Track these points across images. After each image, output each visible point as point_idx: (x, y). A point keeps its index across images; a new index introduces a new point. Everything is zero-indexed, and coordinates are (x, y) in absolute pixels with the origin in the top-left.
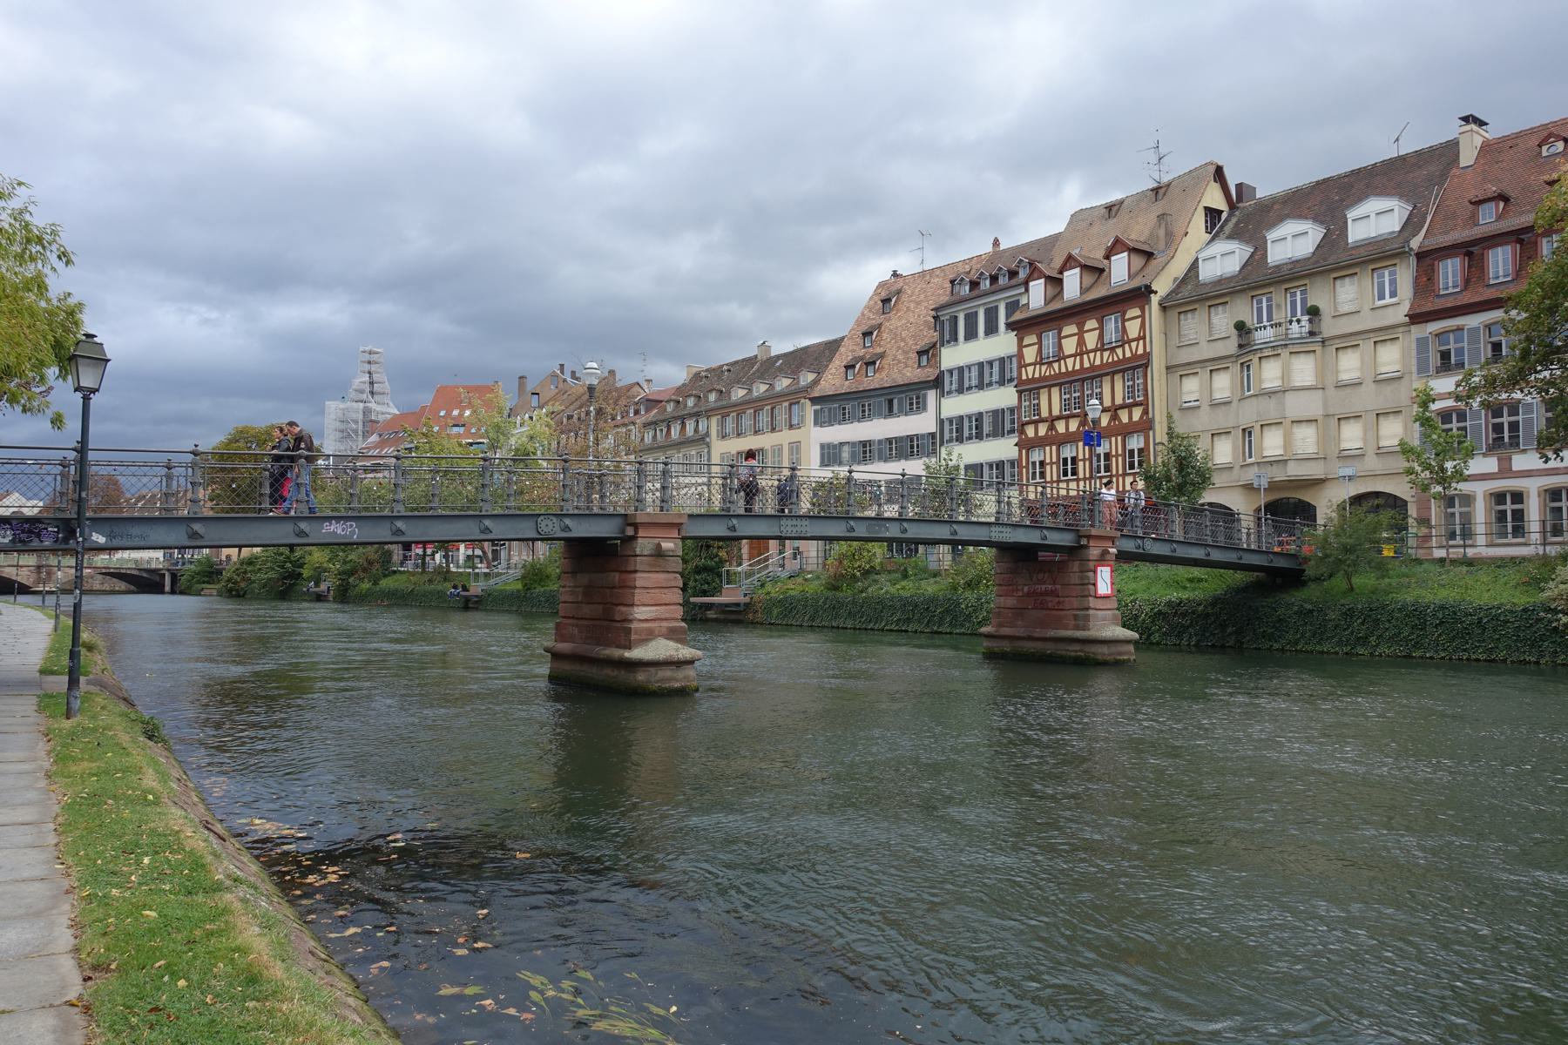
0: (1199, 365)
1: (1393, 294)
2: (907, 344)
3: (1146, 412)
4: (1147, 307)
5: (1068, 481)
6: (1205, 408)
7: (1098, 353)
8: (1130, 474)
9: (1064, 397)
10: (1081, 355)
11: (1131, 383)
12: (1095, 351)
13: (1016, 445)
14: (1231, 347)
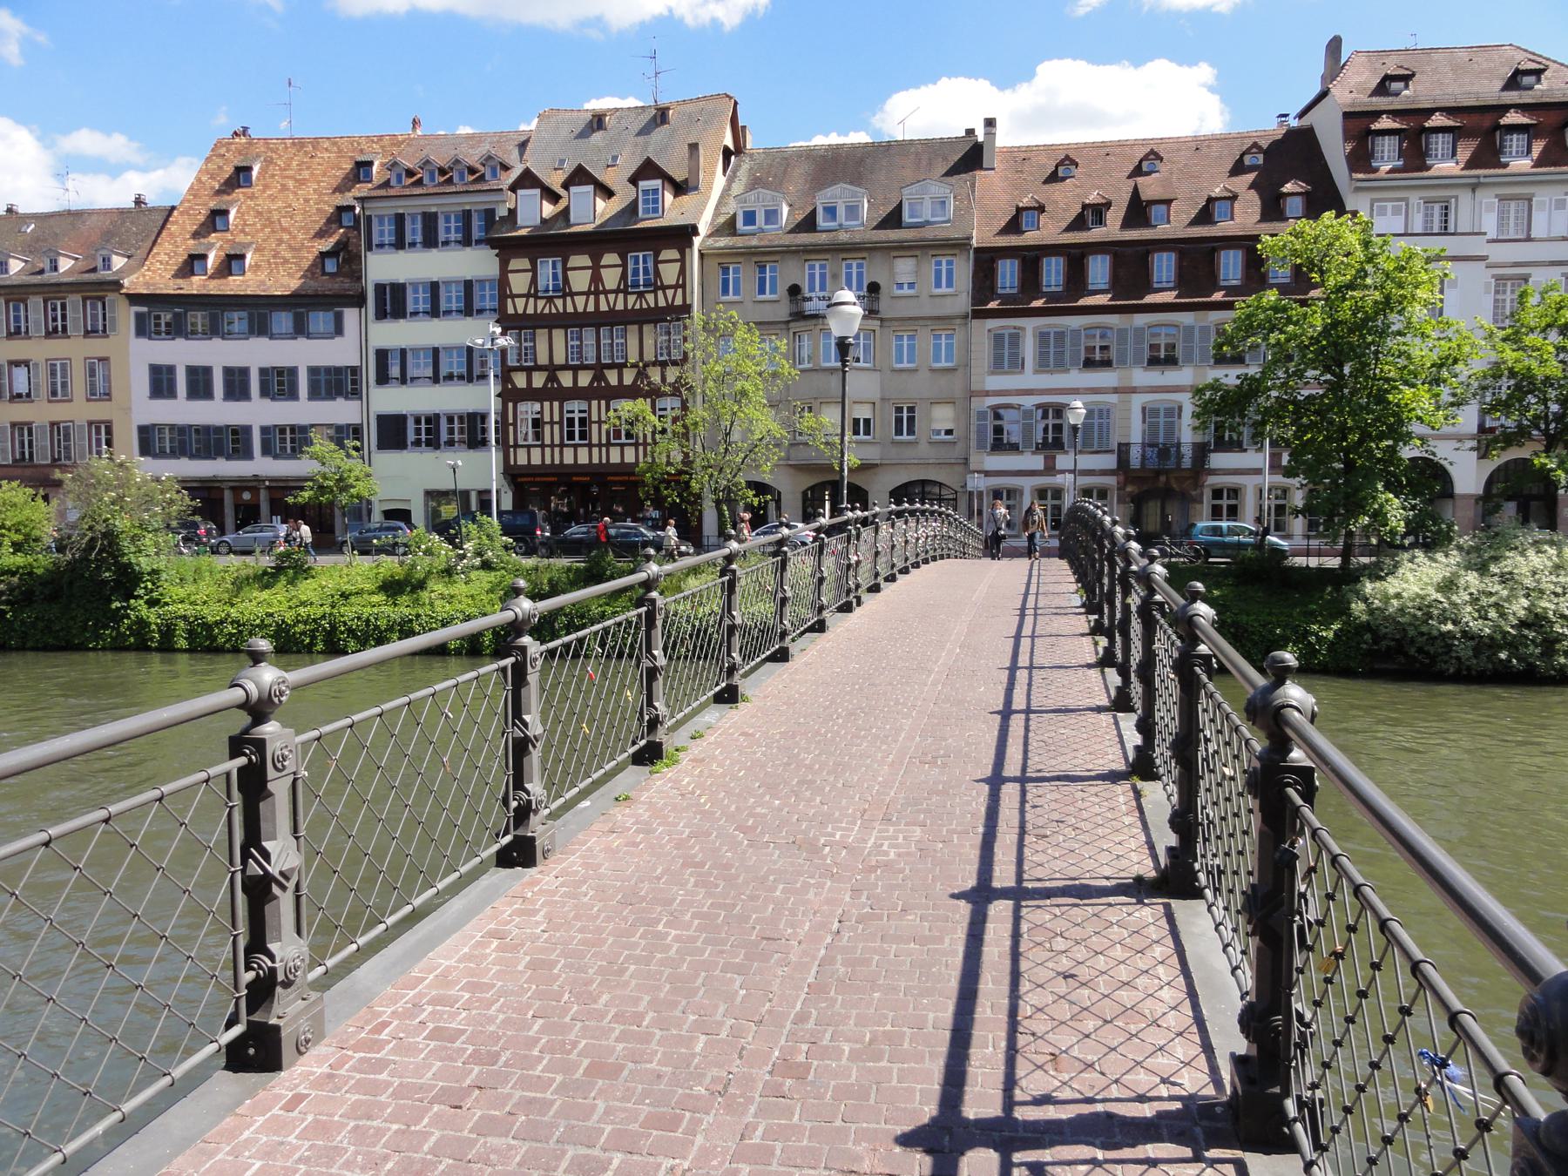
1: (950, 284)
2: (295, 237)
4: (687, 250)
5: (576, 446)
7: (621, 296)
8: (522, 446)
9: (570, 343)
10: (597, 293)
11: (529, 344)
12: (617, 291)
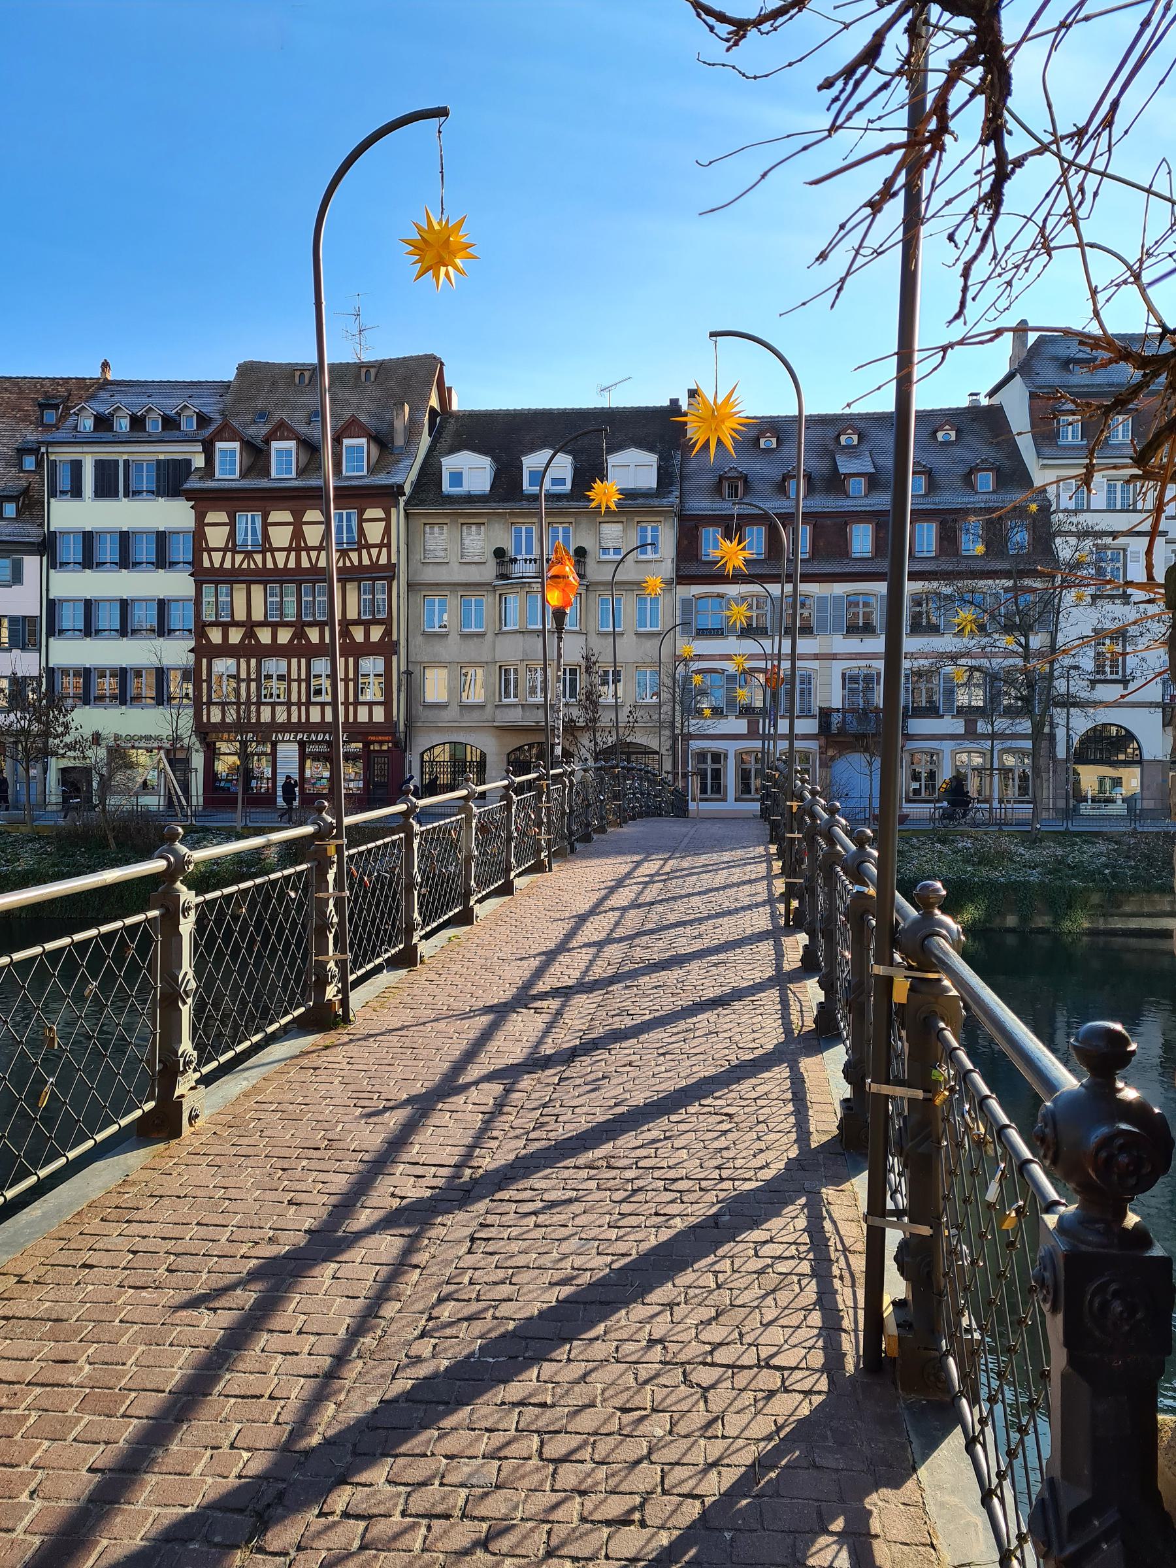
0: (449, 588)
3: (388, 632)
6: (454, 638)
13: (191, 651)
14: (488, 572)
